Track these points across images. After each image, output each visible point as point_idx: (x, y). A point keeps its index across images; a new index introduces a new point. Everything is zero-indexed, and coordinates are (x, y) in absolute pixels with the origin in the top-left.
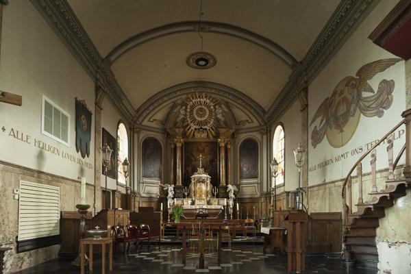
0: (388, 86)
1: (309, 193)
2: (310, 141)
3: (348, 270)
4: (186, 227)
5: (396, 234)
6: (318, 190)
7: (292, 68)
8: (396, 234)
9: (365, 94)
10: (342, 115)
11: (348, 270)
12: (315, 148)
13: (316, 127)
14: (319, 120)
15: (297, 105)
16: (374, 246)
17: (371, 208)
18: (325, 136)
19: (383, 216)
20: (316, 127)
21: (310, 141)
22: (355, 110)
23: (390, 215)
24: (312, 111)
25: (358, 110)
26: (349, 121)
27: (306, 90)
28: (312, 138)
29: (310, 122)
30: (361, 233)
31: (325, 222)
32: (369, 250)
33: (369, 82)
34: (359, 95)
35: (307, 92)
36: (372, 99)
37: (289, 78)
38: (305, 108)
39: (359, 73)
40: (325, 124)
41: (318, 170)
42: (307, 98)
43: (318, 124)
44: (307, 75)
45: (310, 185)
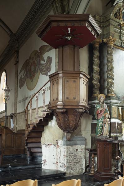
0: (50, 59)
1: (18, 117)
2: (19, 84)
3: (28, 162)
4: (87, 165)
5: (48, 140)
6: (22, 115)
7: (10, 36)
8: (48, 140)
9: (42, 62)
10: (33, 71)
11: (28, 162)
12: (20, 89)
13: (21, 76)
14: (23, 72)
15: (13, 61)
16: (41, 148)
17: (35, 126)
18: (25, 83)
19: (44, 130)
20: (21, 76)
21: (19, 84)
22: (38, 70)
23: (46, 130)
24: (20, 66)
25: (39, 71)
26: (36, 75)
27: (17, 52)
28: (20, 83)
29: (19, 73)
30: (34, 140)
31: (21, 135)
32: (38, 150)
33: (43, 55)
34: (40, 62)
35: (18, 54)
36: (44, 65)
37: (9, 42)
38: (17, 63)
39: (40, 50)
40: (25, 76)
41: (22, 103)
42: (18, 57)
43: (22, 75)
44: (19, 43)
45: (18, 112)
